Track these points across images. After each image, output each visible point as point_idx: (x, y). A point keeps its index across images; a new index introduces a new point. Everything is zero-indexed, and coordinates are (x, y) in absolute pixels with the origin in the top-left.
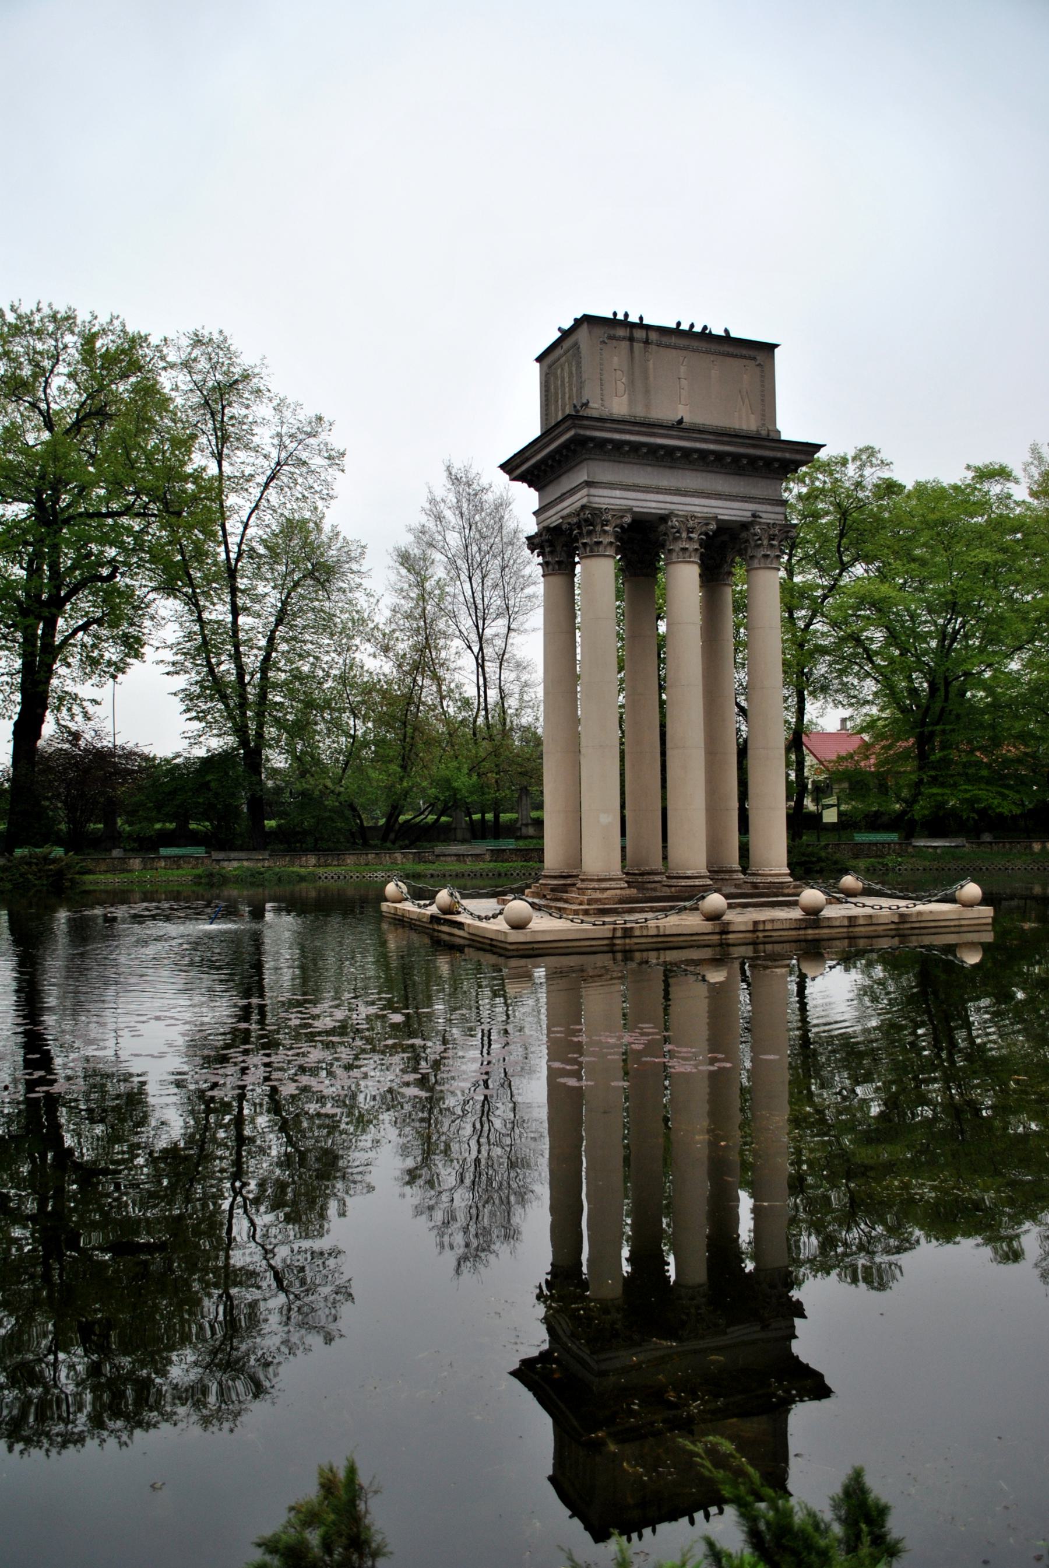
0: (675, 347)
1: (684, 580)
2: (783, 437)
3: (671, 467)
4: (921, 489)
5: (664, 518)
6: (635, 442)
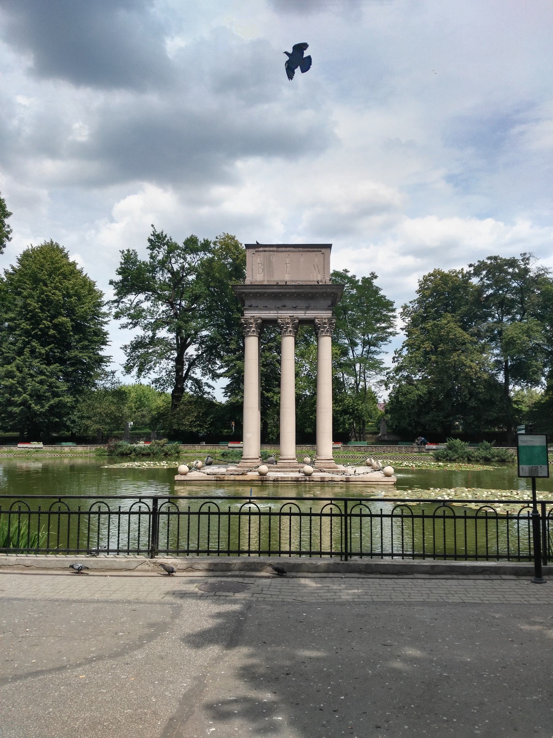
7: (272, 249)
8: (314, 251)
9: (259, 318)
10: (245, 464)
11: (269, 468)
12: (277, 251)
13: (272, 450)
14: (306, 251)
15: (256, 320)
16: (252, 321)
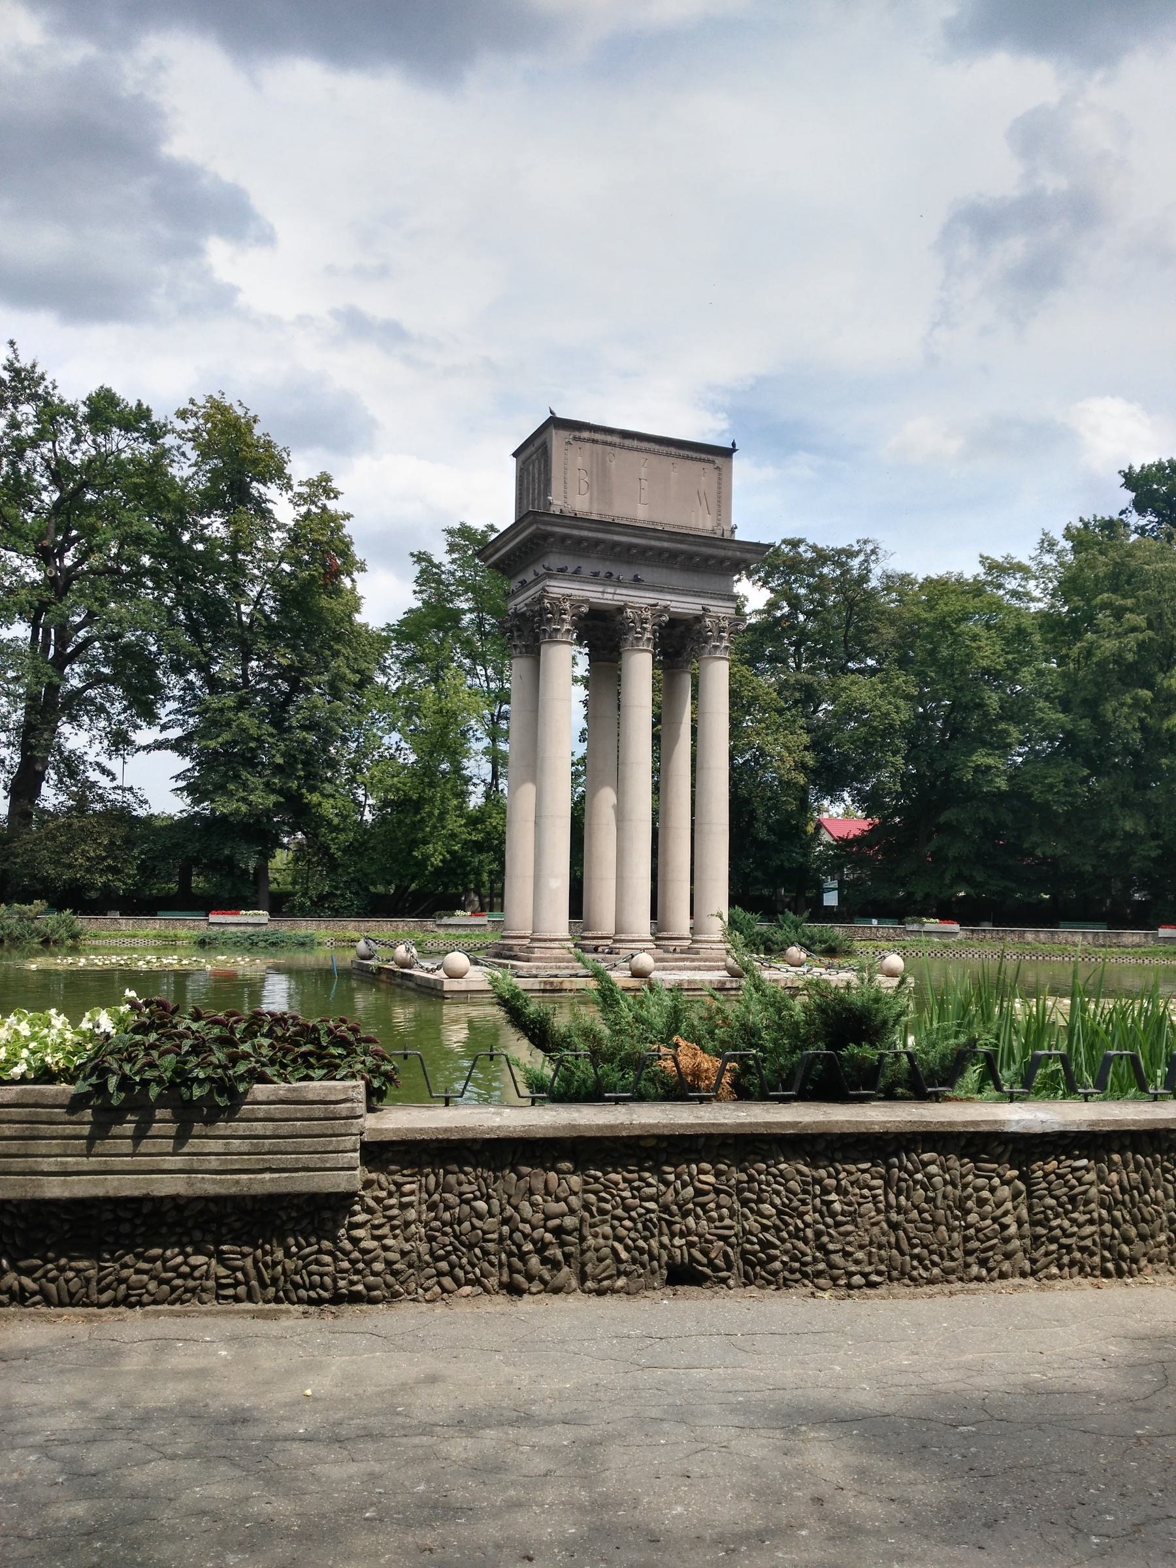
1: (640, 667)
2: (739, 536)
3: (721, 574)
4: (928, 581)
5: (621, 610)
6: (610, 540)
7: (609, 438)
8: (700, 460)
9: (582, 601)
10: (548, 953)
11: (656, 960)
12: (622, 447)
13: (323, 932)
14: (683, 457)
15: (577, 604)
16: (567, 605)
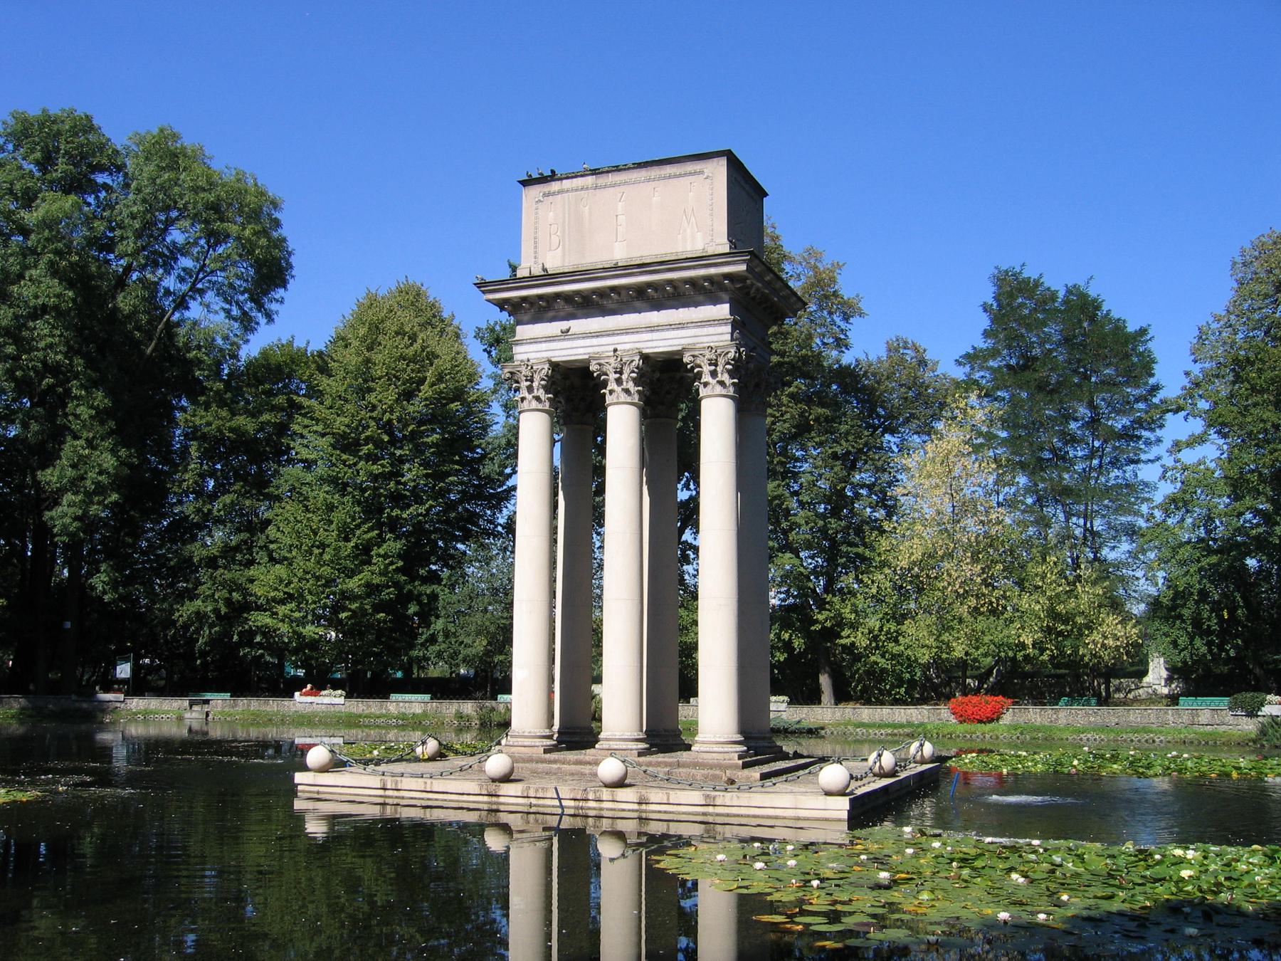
0: (614, 185)
8: (685, 175)
